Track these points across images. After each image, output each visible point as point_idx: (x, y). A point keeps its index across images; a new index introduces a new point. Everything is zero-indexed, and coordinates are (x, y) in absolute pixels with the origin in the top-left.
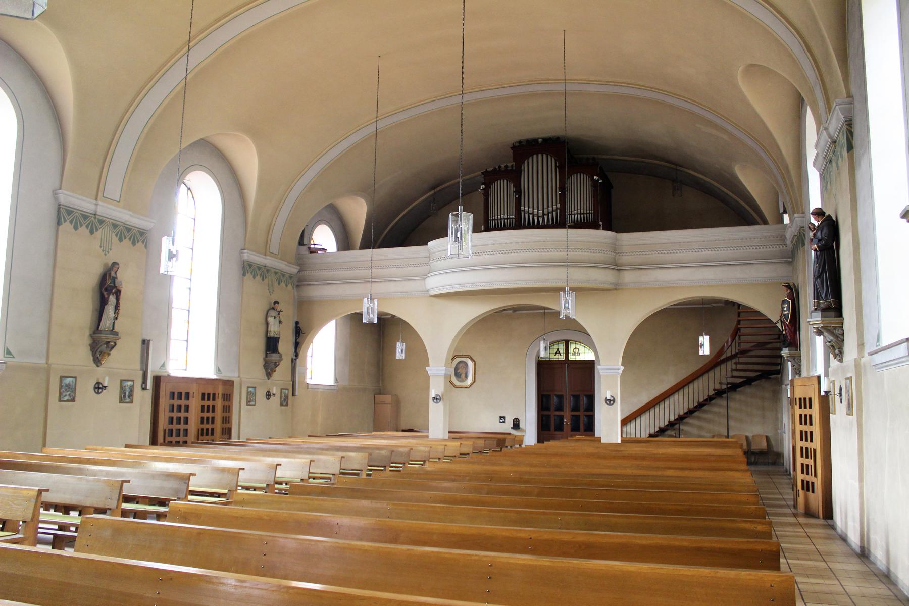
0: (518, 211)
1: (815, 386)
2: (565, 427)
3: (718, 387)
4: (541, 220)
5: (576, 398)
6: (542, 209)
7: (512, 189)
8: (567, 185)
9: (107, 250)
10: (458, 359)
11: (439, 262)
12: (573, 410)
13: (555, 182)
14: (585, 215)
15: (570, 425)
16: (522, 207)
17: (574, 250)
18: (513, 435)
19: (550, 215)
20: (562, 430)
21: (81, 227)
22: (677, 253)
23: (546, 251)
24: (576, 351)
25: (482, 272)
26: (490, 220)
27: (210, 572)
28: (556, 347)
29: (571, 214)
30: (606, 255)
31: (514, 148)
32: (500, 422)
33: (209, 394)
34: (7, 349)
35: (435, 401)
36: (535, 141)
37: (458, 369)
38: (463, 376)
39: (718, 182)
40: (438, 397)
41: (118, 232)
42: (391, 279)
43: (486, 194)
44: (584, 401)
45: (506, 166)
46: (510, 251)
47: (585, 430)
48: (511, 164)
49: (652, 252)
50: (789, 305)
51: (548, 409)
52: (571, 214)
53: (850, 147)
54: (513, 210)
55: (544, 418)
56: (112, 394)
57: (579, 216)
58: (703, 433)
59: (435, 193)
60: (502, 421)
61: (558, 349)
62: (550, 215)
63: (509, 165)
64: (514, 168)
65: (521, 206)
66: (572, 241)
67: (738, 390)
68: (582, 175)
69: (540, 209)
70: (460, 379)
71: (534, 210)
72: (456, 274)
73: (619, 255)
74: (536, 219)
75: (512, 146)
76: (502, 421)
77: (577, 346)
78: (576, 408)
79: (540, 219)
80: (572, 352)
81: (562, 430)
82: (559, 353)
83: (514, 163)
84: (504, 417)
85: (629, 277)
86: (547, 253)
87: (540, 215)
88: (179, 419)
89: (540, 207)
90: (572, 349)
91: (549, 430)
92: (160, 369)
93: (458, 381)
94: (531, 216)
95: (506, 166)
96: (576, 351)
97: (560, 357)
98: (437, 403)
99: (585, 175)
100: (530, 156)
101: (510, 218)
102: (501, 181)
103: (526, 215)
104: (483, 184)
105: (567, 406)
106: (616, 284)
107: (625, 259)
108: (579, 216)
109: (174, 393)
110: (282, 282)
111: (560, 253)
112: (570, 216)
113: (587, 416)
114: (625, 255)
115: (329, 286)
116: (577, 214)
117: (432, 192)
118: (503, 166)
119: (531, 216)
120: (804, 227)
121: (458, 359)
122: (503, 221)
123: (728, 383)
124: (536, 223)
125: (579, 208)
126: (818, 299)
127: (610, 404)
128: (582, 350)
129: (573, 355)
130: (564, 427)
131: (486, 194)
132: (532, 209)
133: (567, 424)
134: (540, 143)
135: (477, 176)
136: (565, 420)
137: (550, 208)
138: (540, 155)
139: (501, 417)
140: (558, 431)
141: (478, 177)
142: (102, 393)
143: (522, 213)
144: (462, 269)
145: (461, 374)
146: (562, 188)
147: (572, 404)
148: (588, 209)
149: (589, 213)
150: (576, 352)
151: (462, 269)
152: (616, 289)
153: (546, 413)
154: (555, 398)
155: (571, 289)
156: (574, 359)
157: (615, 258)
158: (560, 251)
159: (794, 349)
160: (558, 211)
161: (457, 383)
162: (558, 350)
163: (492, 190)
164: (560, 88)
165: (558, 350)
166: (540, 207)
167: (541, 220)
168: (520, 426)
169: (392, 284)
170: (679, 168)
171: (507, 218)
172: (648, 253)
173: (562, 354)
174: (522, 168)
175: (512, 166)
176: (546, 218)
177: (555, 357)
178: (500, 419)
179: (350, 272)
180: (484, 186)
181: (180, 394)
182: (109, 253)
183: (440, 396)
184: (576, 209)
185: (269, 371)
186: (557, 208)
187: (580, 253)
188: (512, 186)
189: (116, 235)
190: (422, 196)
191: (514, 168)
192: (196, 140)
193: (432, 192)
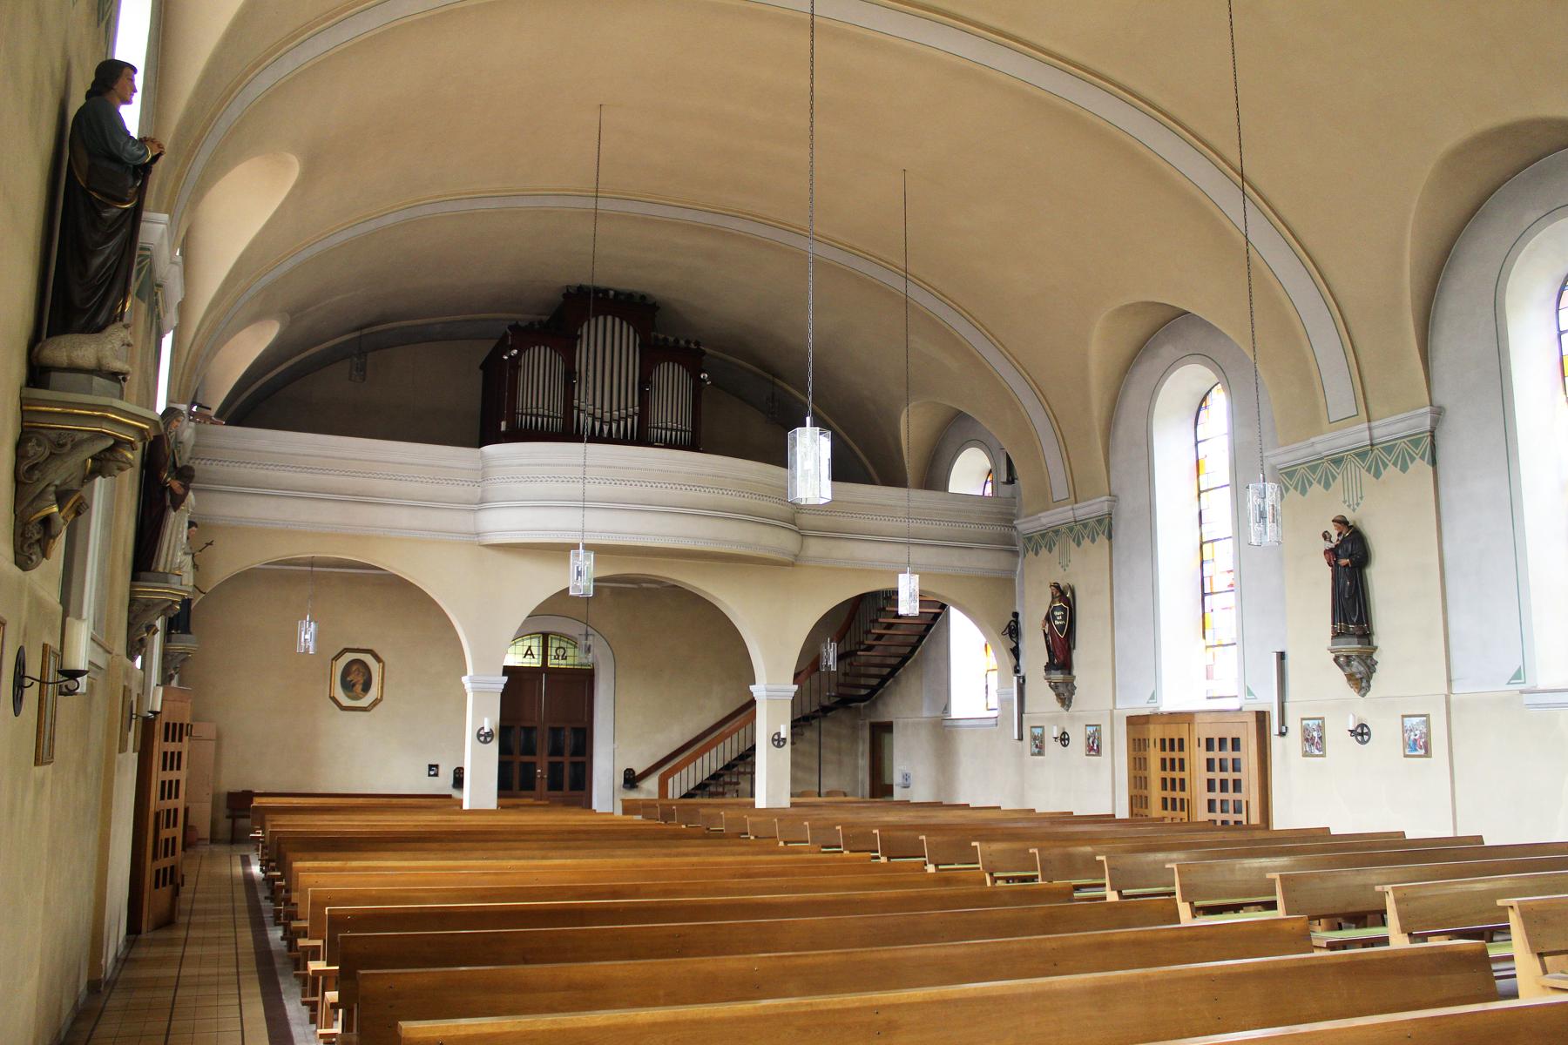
0: (643, 415)
1: (1249, 724)
2: (538, 783)
4: (606, 428)
5: (556, 732)
7: (560, 366)
8: (655, 377)
9: (1355, 502)
11: (522, 485)
12: (552, 754)
13: (634, 373)
15: (546, 780)
16: (576, 402)
19: (622, 423)
21: (1412, 462)
24: (561, 652)
25: (627, 515)
26: (518, 413)
27: (1214, 1040)
28: (527, 643)
32: (429, 775)
33: (1172, 741)
34: (1248, 688)
37: (348, 675)
41: (1398, 456)
47: (555, 784)
50: (1065, 613)
53: (1434, 462)
54: (561, 404)
56: (1386, 732)
57: (669, 433)
59: (360, 337)
60: (432, 773)
61: (530, 647)
62: (622, 423)
67: (829, 714)
69: (605, 410)
70: (350, 694)
71: (596, 410)
72: (690, 519)
75: (565, 291)
76: (432, 773)
78: (556, 750)
80: (554, 653)
82: (532, 654)
84: (437, 766)
85: (815, 548)
88: (1224, 783)
90: (554, 650)
92: (1148, 703)
93: (349, 697)
96: (561, 652)
97: (533, 660)
98: (485, 742)
101: (553, 417)
102: (668, 365)
105: (543, 743)
108: (669, 433)
109: (1164, 740)
110: (1041, 547)
115: (262, 500)
117: (357, 334)
120: (1111, 514)
124: (597, 432)
126: (1346, 622)
129: (555, 659)
130: (537, 784)
132: (600, 411)
133: (542, 778)
138: (609, 318)
139: (431, 767)
142: (1369, 743)
143: (575, 412)
144: (771, 521)
145: (354, 685)
146: (645, 381)
148: (551, 409)
150: (561, 654)
151: (771, 521)
153: (558, 759)
155: (588, 547)
156: (528, 665)
159: (1067, 672)
160: (636, 418)
161: (346, 702)
167: (606, 428)
173: (536, 656)
176: (614, 426)
177: (525, 660)
179: (305, 475)
181: (1222, 741)
182: (1361, 505)
184: (664, 421)
185: (173, 672)
188: (559, 360)
189: (1074, 540)
192: (1177, 306)
193: (357, 334)
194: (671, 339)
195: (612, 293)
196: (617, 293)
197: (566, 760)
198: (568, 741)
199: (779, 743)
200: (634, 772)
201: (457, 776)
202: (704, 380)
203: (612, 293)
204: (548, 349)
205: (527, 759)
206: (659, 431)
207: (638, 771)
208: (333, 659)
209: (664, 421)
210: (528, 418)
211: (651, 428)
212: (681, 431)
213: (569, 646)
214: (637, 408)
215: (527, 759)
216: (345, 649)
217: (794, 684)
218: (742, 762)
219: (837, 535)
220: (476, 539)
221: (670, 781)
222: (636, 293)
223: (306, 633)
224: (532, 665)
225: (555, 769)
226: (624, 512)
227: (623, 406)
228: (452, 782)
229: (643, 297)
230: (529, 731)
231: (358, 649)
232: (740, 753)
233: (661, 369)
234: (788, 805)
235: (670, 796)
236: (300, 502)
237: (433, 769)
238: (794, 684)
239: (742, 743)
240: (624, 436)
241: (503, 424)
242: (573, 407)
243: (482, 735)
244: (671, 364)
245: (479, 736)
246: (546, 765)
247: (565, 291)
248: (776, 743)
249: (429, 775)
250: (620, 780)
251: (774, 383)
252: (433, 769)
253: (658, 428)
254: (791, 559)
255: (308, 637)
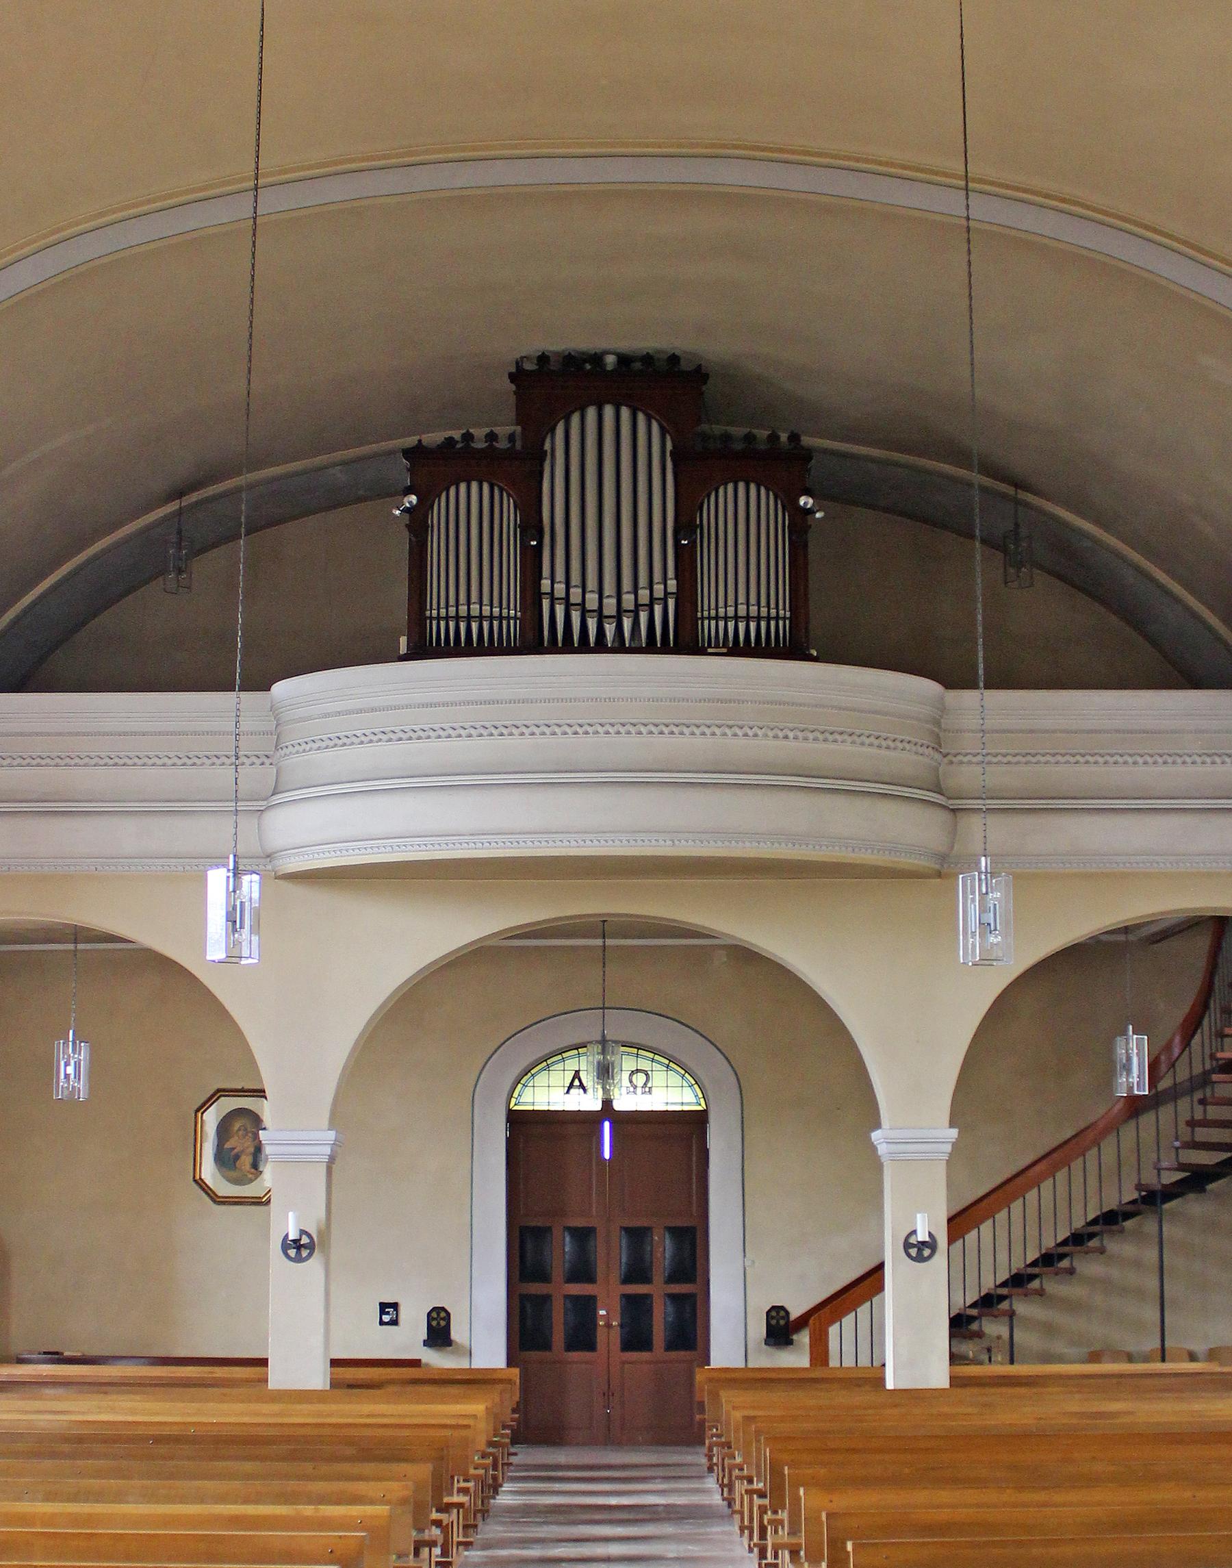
0: (532, 595)
2: (601, 1336)
3: (1150, 1178)
4: (610, 629)
5: (637, 1236)
6: (613, 593)
7: (510, 515)
8: (707, 516)
10: (228, 1104)
11: (330, 753)
12: (628, 1279)
14: (763, 624)
16: (546, 584)
17: (831, 738)
18: (427, 1365)
19: (643, 616)
20: (591, 1346)
22: (1135, 763)
23: (740, 733)
24: (640, 1079)
25: (514, 796)
26: (431, 618)
28: (572, 1065)
29: (717, 618)
30: (921, 758)
31: (518, 376)
32: (382, 1323)
35: (292, 1252)
36: (597, 359)
38: (246, 1161)
39: (1149, 553)
40: (305, 1240)
42: (118, 806)
43: (418, 523)
44: (663, 1250)
45: (491, 437)
46: (613, 725)
48: (510, 429)
49: (1059, 758)
51: (542, 1276)
52: (717, 618)
55: (528, 1306)
57: (742, 626)
58: (1060, 1347)
59: (180, 512)
60: (386, 1318)
61: (577, 1072)
63: (503, 431)
64: (518, 445)
65: (540, 578)
66: (824, 706)
67: (1210, 1187)
68: (753, 487)
69: (606, 593)
70: (233, 1174)
71: (588, 596)
73: (951, 763)
74: (592, 624)
77: (644, 1064)
78: (637, 1272)
79: (607, 626)
81: (591, 1346)
82: (582, 1086)
83: (519, 429)
84: (395, 1306)
86: (742, 741)
87: (606, 612)
89: (609, 588)
90: (626, 1076)
91: (546, 1346)
94: (576, 616)
95: (491, 437)
98: (299, 1259)
99: (763, 491)
100: (576, 410)
101: (501, 618)
103: (560, 610)
104: (408, 491)
106: (943, 858)
107: (966, 776)
108: (742, 626)
111: (784, 742)
112: (713, 623)
113: (674, 1298)
114: (970, 763)
116: (736, 618)
117: (172, 507)
118: (479, 433)
119: (576, 616)
121: (228, 1104)
122: (474, 626)
123: (1182, 1167)
125: (742, 599)
127: (920, 1258)
128: (660, 1077)
131: (418, 523)
132: (563, 586)
133: (608, 1326)
134: (609, 368)
135: (334, 465)
136: (602, 1312)
137: (644, 595)
138: (609, 411)
139: (384, 1307)
140: (529, 1349)
141: (331, 471)
143: (546, 603)
144: (839, 784)
145: (237, 1157)
147: (624, 1260)
149: (777, 618)
152: (939, 875)
153: (535, 1288)
154: (568, 1239)
156: (530, 1108)
157: (937, 769)
158: (786, 737)
161: (225, 1189)
162: (577, 1075)
163: (437, 515)
164: (950, 204)
165: (577, 1075)
166: (609, 588)
168: (455, 1335)
169: (129, 825)
170: (1022, 495)
171: (481, 618)
172: (1042, 759)
174: (547, 446)
175: (511, 438)
176: (627, 623)
178: (382, 1312)
180: (414, 498)
183: (309, 1236)
184: (731, 601)
186: (666, 593)
187: (849, 748)
188: (509, 505)
190: (135, 515)
191: (518, 445)
193: (172, 507)
194: (762, 434)
195: (610, 360)
196: (624, 360)
197: (657, 1289)
198: (663, 1250)
199: (920, 1251)
200: (787, 1313)
201: (774, 1322)
202: (810, 512)
203: (610, 360)
204: (486, 487)
205: (576, 1289)
206: (721, 624)
207: (795, 1312)
208: (197, 1111)
209: (731, 601)
210: (452, 624)
211: (703, 618)
212: (769, 619)
213: (656, 1066)
214: (672, 585)
215: (576, 1289)
216: (219, 1091)
217: (952, 1125)
218: (1020, 1290)
219: (61, 806)
220: (269, 867)
221: (833, 1330)
222: (659, 352)
223: (67, 1064)
224: (536, 1108)
225: (636, 1308)
226: (424, 788)
227: (643, 581)
228: (425, 1337)
229: (674, 359)
230: (583, 1236)
231: (243, 1090)
232: (1014, 1271)
233: (721, 500)
234: (944, 1383)
235: (834, 1362)
236: (1087, 819)
237: (389, 1311)
238: (952, 1125)
239: (1017, 1248)
240: (756, 644)
241: (403, 640)
242: (538, 596)
243: (913, 1246)
244: (741, 485)
245: (907, 1245)
246: (617, 1305)
247: (514, 370)
248: (913, 1252)
249: (382, 1323)
250: (759, 1329)
251: (1018, 502)
252: (389, 1311)
253: (457, 618)
254: (933, 865)
255: (70, 1070)
